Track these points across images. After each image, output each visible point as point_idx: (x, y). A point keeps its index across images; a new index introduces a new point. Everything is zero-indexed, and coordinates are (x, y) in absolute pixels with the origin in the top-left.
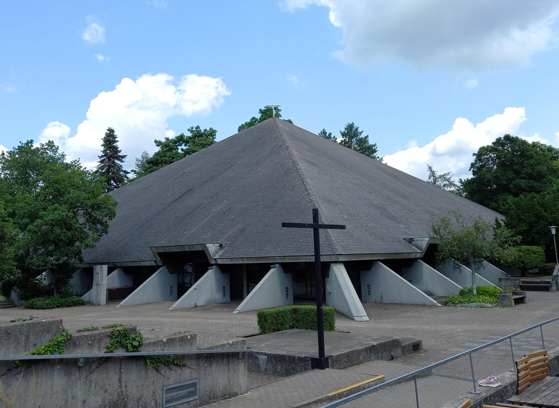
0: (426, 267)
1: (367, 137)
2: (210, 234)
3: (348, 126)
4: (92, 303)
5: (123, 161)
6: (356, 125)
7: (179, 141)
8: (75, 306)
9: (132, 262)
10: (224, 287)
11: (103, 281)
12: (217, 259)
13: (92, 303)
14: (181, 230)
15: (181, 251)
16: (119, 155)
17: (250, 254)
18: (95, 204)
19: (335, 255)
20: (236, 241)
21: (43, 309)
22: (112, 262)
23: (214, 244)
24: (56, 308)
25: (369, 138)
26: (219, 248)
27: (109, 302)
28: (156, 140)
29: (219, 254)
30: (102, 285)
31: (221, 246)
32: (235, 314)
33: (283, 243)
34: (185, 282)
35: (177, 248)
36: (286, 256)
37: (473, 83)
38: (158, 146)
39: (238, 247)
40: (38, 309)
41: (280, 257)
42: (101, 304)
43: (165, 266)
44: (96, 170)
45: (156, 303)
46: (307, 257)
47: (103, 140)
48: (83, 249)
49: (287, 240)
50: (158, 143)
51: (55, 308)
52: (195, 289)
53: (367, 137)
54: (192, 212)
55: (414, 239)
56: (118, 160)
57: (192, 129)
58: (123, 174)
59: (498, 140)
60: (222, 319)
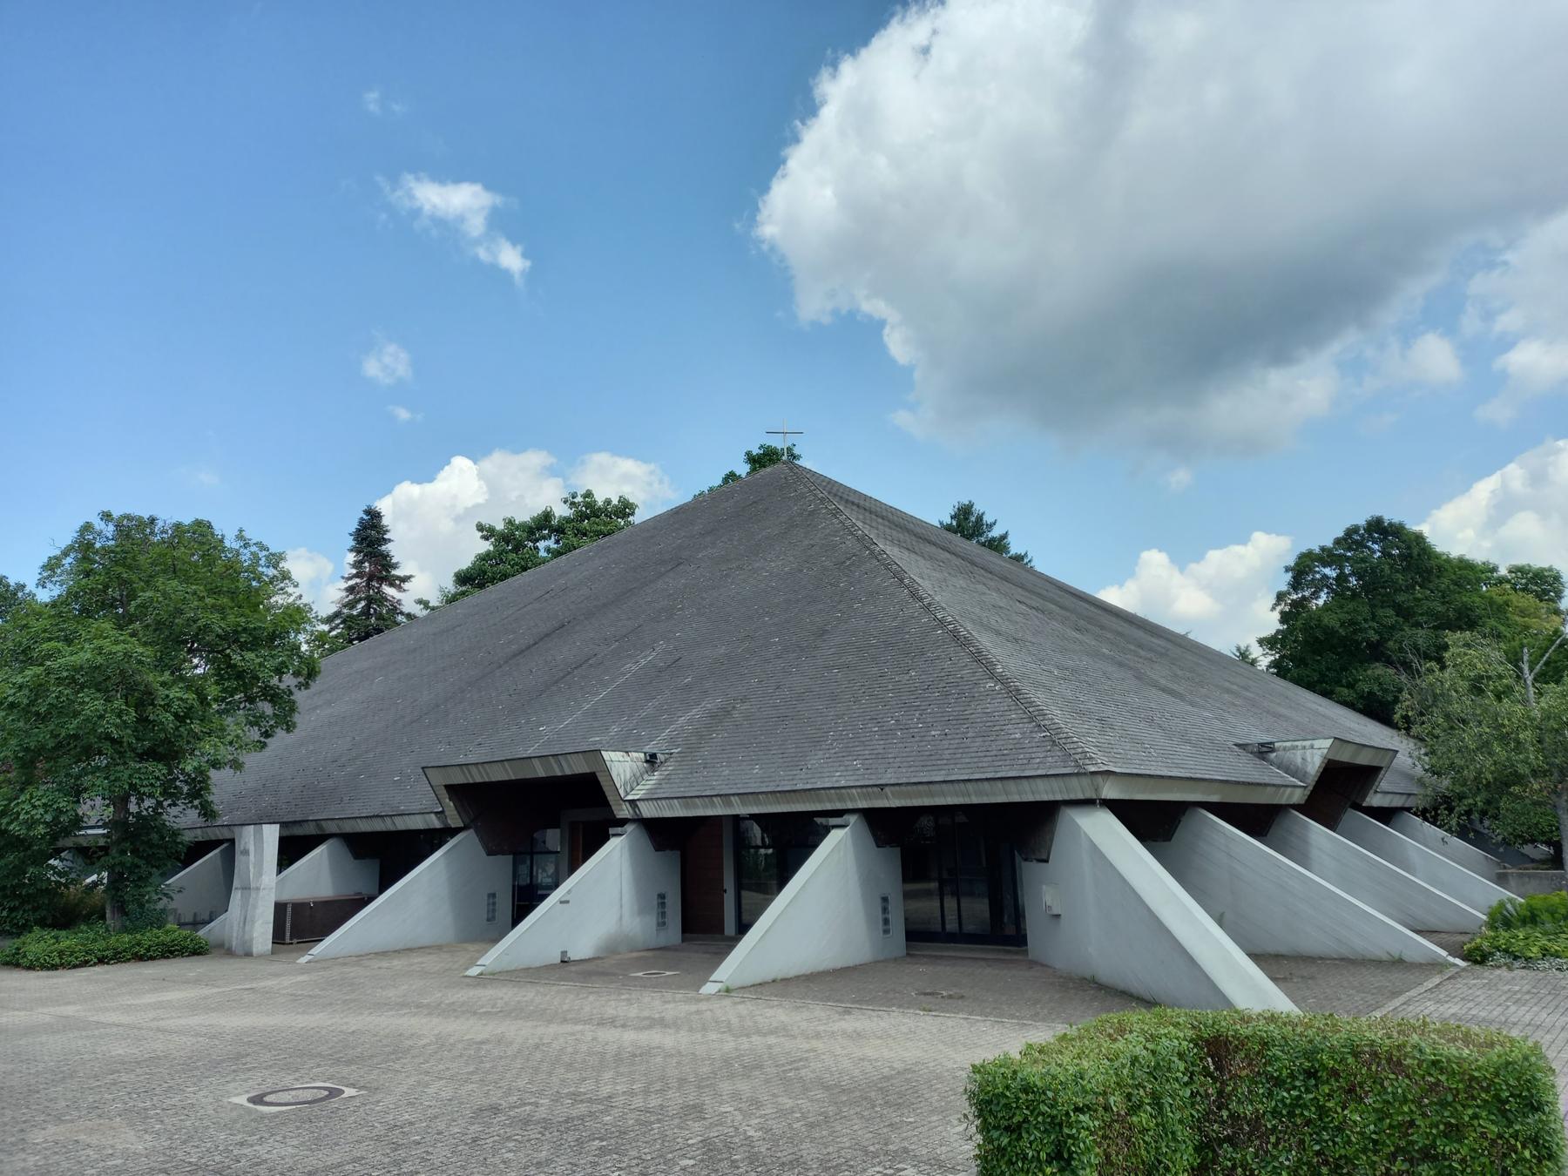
0: (1317, 830)
1: (1004, 537)
2: (615, 729)
3: (958, 509)
4: (226, 947)
5: (404, 590)
6: (978, 508)
7: (540, 528)
8: (168, 957)
9: (371, 817)
10: (662, 896)
11: (261, 875)
12: (638, 800)
13: (226, 947)
14: (527, 722)
15: (520, 777)
16: (393, 576)
17: (753, 781)
18: (245, 630)
19: (1085, 774)
20: (702, 745)
21: (48, 969)
22: (312, 820)
23: (627, 752)
24: (95, 964)
25: (1010, 539)
26: (645, 764)
27: (292, 943)
28: (481, 525)
29: (643, 785)
30: (258, 889)
31: (651, 759)
32: (708, 998)
33: (867, 743)
34: (539, 881)
35: (506, 771)
36: (887, 785)
37: (1181, 477)
38: (486, 538)
39: (708, 761)
40: (31, 968)
41: (864, 790)
42: (255, 950)
43: (472, 830)
44: (336, 609)
45: (438, 948)
46: (970, 786)
47: (352, 537)
48: (52, 727)
49: (879, 733)
50: (487, 532)
51: (91, 966)
52: (561, 902)
53: (1004, 537)
54: (564, 677)
55: (1276, 744)
56: (392, 585)
57: (573, 498)
58: (404, 620)
59: (1352, 531)
60: (662, 1023)
